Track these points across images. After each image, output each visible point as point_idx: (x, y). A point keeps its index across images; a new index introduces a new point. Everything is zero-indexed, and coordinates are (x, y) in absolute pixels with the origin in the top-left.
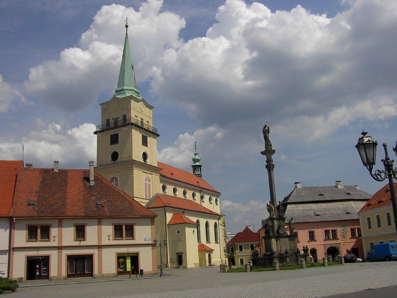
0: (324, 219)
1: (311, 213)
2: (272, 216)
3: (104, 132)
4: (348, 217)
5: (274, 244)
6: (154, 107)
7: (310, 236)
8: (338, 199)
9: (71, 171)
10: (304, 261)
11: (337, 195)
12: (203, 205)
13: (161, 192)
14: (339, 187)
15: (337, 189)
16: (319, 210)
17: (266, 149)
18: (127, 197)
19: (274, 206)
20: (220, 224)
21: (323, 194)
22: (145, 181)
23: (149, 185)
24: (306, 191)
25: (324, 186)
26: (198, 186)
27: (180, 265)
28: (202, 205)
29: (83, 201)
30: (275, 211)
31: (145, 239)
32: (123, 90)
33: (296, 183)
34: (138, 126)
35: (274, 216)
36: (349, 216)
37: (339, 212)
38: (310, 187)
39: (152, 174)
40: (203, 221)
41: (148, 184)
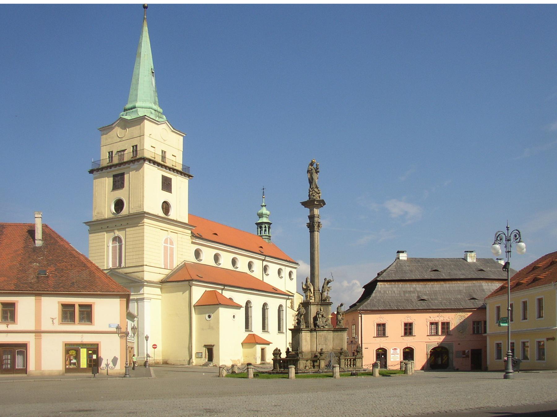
2: (308, 299)
3: (104, 171)
5: (306, 341)
6: (124, 151)
7: (405, 329)
8: (462, 277)
9: (10, 225)
10: (337, 367)
12: (267, 280)
13: (193, 259)
14: (469, 260)
16: (428, 293)
17: (310, 198)
18: (89, 265)
19: (313, 286)
20: (288, 307)
22: (164, 243)
23: (172, 249)
24: (413, 265)
25: (445, 258)
26: (260, 253)
27: (210, 362)
28: (264, 281)
29: (18, 268)
30: (314, 293)
31: (109, 325)
32: (135, 107)
33: (398, 252)
34: (155, 163)
35: (311, 299)
39: (177, 233)
40: (257, 301)
41: (170, 247)
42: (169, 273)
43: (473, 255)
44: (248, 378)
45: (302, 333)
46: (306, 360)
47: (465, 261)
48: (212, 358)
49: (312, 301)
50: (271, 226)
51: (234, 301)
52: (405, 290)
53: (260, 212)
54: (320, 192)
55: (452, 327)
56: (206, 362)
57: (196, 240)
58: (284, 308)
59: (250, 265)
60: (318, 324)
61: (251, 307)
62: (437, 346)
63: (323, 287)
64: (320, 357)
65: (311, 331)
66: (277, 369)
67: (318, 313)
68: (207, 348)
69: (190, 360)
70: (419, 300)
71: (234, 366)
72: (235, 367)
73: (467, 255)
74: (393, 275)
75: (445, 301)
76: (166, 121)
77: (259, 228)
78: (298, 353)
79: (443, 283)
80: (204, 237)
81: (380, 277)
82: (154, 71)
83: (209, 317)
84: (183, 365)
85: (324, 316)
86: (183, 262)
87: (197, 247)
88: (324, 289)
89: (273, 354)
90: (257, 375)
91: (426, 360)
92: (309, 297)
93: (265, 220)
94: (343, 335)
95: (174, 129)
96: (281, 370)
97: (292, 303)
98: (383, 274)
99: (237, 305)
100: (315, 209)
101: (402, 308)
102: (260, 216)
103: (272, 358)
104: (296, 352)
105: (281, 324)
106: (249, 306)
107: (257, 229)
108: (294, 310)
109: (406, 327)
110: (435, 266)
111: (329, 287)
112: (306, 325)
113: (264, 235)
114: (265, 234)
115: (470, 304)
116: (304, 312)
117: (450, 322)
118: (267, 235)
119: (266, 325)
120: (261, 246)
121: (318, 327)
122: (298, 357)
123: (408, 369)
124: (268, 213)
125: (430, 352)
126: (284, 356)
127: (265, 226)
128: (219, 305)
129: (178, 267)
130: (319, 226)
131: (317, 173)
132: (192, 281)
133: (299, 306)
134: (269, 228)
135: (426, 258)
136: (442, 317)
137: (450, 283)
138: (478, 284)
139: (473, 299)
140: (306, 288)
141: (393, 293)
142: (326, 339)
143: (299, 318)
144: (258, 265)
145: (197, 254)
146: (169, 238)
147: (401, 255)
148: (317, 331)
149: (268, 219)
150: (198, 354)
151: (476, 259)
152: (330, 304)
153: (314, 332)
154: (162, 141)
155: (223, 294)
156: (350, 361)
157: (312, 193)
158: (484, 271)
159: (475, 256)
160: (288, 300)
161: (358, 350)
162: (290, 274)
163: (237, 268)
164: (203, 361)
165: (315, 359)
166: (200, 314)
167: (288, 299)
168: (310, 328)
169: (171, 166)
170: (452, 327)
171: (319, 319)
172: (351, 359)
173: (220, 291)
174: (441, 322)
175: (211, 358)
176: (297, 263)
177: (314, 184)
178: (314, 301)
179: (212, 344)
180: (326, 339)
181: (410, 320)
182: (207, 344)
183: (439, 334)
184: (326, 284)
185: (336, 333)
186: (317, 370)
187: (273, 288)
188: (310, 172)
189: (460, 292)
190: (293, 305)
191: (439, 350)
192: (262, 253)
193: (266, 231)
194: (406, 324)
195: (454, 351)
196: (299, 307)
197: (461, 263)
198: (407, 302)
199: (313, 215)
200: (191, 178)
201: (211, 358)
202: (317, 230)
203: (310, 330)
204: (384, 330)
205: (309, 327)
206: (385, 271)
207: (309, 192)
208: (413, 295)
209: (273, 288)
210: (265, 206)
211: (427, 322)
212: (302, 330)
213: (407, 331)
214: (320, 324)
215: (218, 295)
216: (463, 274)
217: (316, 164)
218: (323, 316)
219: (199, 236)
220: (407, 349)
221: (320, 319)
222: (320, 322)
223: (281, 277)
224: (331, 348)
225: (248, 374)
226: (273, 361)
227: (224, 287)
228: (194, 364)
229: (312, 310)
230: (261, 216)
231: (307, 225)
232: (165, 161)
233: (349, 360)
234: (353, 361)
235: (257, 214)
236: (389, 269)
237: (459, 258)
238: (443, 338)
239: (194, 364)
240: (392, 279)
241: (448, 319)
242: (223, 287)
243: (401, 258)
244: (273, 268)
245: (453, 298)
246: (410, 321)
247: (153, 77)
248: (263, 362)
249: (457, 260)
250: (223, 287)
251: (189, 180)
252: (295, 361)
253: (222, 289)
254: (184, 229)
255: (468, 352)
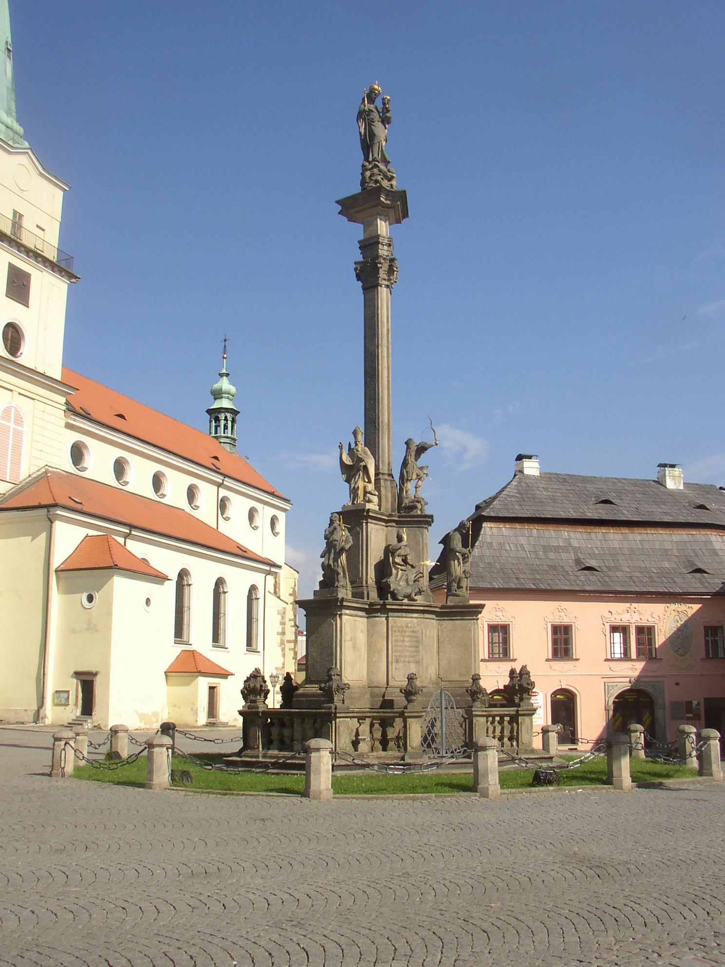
0: (611, 584)
1: (568, 559)
4: (699, 585)
5: (355, 647)
7: (555, 642)
8: (667, 519)
11: (663, 506)
12: (225, 528)
13: (66, 464)
14: (670, 484)
15: (662, 488)
21: (613, 501)
25: (618, 477)
26: (214, 468)
28: (219, 530)
30: (377, 481)
35: (370, 501)
36: (702, 583)
37: (666, 565)
38: (568, 475)
41: (15, 430)
42: (8, 492)
43: (678, 472)
44: (150, 787)
45: (344, 617)
46: (359, 718)
47: (661, 486)
48: (92, 708)
49: (373, 506)
50: (237, 418)
51: (151, 565)
52: (546, 544)
53: (216, 386)
54: (395, 175)
55: (660, 639)
56: (77, 717)
57: (75, 420)
58: (260, 594)
59: (191, 493)
60: (393, 587)
61: (190, 585)
62: (629, 688)
63: (405, 464)
64: (406, 707)
65: (371, 611)
66: (258, 748)
67: (389, 551)
68: (81, 680)
69: (38, 711)
70: (581, 570)
71: (116, 732)
72: (120, 734)
73: (665, 474)
74: (517, 507)
75: (638, 574)
76: (28, 149)
77: (214, 421)
78: (331, 687)
79: (627, 532)
80: (94, 415)
81: (488, 510)
82: (12, 48)
83: (90, 599)
84: (23, 723)
85: (409, 561)
86: (42, 468)
87: (76, 437)
88: (407, 472)
89: (242, 692)
90: (185, 774)
91: (603, 724)
92: (361, 493)
93: (225, 403)
94: (470, 630)
95: (44, 169)
96: (270, 752)
97: (276, 586)
98: (495, 503)
99: (157, 573)
100: (378, 219)
101: (546, 585)
102: (217, 396)
103: (241, 708)
104: (323, 685)
105: (254, 636)
106: (185, 583)
107: (209, 424)
108: (279, 598)
109: (556, 637)
110: (601, 492)
111: (421, 468)
112: (355, 591)
113: (223, 435)
114: (224, 433)
115: (694, 584)
116: (346, 541)
117: (654, 626)
118: (229, 435)
119: (221, 632)
120: (216, 455)
121: (394, 597)
122: (333, 706)
123: (713, 759)
124: (233, 389)
125: (614, 702)
126: (274, 701)
127: (226, 417)
128: (114, 568)
129: (30, 478)
130: (391, 271)
131: (383, 122)
132: (56, 508)
133: (332, 522)
134: (233, 421)
135: (579, 476)
136: (637, 614)
137: (643, 530)
138: (703, 538)
139: (699, 571)
140: (352, 464)
141: (519, 548)
142: (417, 642)
143: (331, 562)
144: (208, 495)
145: (77, 453)
146: (13, 409)
147: (527, 463)
148: (390, 614)
149: (231, 402)
150: (58, 694)
151: (684, 483)
152: (427, 521)
153: (379, 614)
154: (17, 191)
155: (128, 547)
156: (501, 722)
157: (372, 175)
158: (707, 509)
159: (682, 476)
160: (268, 576)
161: (525, 685)
162: (273, 521)
163: (163, 496)
164: (70, 714)
165: (387, 713)
166: (69, 594)
167: (269, 573)
168: (366, 600)
169: (33, 248)
170: (660, 639)
171: (394, 571)
172: (502, 717)
173: (121, 540)
174: (636, 626)
175: (88, 708)
176: (287, 500)
177: (376, 148)
178: (378, 507)
179: (94, 670)
180: (417, 641)
181: (565, 618)
182: (80, 669)
183: (632, 658)
184: (413, 454)
185: (448, 624)
186: (396, 758)
187: (238, 547)
188: (364, 120)
189: (665, 553)
190: (277, 589)
191: (631, 698)
192: (218, 470)
193: (227, 429)
194: (556, 629)
195: (667, 702)
196: (330, 525)
197: (653, 489)
198: (555, 573)
199: (373, 237)
200: (73, 280)
201: (88, 708)
202: (387, 283)
203: (367, 607)
204: (506, 642)
205: (363, 598)
206: (494, 499)
207: (362, 174)
208: (564, 556)
209: (238, 547)
210: (227, 375)
211: (603, 624)
212: (343, 607)
213: (559, 646)
214: (400, 588)
215: (114, 548)
216: (666, 514)
217: (383, 99)
218: (405, 561)
219: (84, 413)
220: (561, 695)
221: (397, 569)
222: (398, 581)
223: (255, 526)
224: (434, 677)
225: (151, 772)
226: (241, 718)
227: (130, 532)
228: (48, 721)
229: (373, 537)
230: (217, 395)
231: (356, 269)
232: (20, 236)
233: (497, 718)
234: (510, 722)
235: (210, 391)
236: (503, 493)
237: (646, 480)
238: (640, 665)
239: (48, 721)
240: (515, 515)
241: (651, 620)
242: (128, 531)
243: (527, 472)
244: (239, 505)
245: (654, 568)
246: (565, 621)
247: (8, 60)
248: (212, 720)
249: (644, 483)
250: (128, 531)
251: (69, 285)
252: (319, 721)
253: (127, 536)
254: (51, 391)
255: (698, 704)
